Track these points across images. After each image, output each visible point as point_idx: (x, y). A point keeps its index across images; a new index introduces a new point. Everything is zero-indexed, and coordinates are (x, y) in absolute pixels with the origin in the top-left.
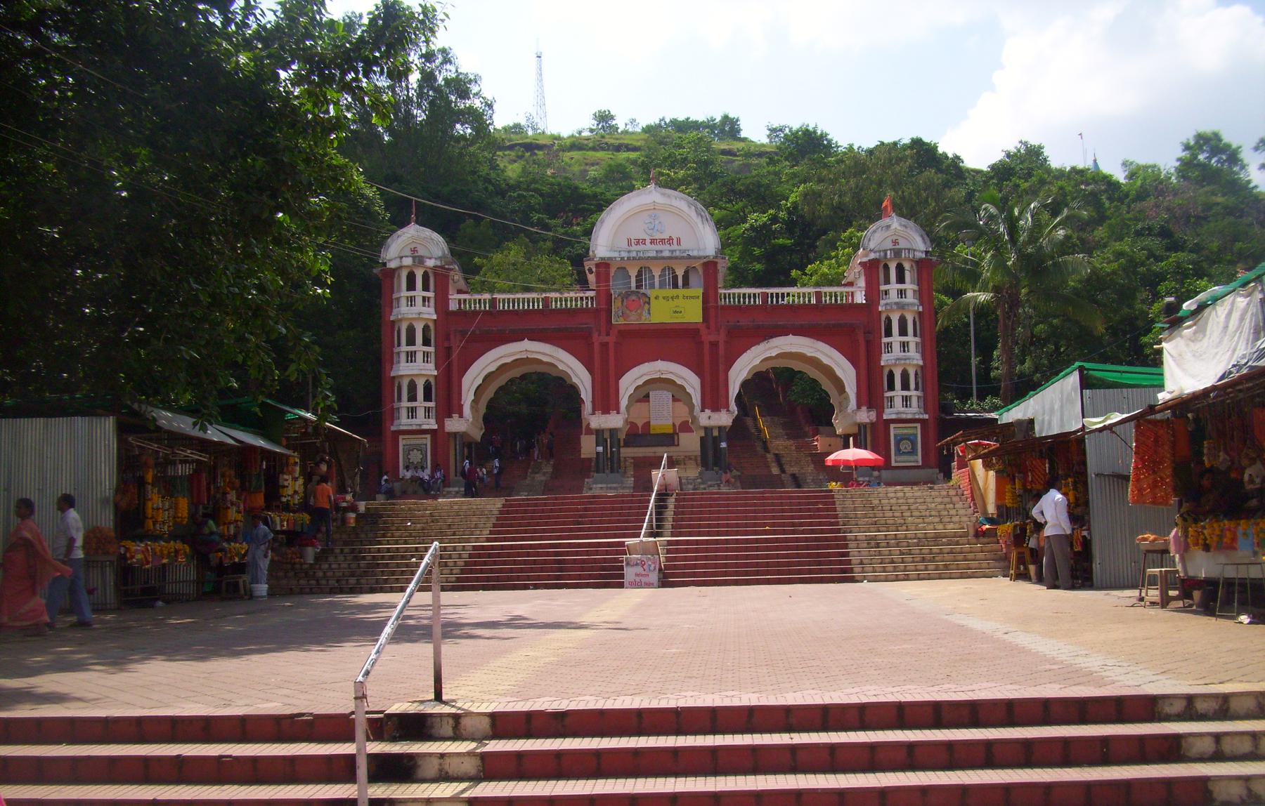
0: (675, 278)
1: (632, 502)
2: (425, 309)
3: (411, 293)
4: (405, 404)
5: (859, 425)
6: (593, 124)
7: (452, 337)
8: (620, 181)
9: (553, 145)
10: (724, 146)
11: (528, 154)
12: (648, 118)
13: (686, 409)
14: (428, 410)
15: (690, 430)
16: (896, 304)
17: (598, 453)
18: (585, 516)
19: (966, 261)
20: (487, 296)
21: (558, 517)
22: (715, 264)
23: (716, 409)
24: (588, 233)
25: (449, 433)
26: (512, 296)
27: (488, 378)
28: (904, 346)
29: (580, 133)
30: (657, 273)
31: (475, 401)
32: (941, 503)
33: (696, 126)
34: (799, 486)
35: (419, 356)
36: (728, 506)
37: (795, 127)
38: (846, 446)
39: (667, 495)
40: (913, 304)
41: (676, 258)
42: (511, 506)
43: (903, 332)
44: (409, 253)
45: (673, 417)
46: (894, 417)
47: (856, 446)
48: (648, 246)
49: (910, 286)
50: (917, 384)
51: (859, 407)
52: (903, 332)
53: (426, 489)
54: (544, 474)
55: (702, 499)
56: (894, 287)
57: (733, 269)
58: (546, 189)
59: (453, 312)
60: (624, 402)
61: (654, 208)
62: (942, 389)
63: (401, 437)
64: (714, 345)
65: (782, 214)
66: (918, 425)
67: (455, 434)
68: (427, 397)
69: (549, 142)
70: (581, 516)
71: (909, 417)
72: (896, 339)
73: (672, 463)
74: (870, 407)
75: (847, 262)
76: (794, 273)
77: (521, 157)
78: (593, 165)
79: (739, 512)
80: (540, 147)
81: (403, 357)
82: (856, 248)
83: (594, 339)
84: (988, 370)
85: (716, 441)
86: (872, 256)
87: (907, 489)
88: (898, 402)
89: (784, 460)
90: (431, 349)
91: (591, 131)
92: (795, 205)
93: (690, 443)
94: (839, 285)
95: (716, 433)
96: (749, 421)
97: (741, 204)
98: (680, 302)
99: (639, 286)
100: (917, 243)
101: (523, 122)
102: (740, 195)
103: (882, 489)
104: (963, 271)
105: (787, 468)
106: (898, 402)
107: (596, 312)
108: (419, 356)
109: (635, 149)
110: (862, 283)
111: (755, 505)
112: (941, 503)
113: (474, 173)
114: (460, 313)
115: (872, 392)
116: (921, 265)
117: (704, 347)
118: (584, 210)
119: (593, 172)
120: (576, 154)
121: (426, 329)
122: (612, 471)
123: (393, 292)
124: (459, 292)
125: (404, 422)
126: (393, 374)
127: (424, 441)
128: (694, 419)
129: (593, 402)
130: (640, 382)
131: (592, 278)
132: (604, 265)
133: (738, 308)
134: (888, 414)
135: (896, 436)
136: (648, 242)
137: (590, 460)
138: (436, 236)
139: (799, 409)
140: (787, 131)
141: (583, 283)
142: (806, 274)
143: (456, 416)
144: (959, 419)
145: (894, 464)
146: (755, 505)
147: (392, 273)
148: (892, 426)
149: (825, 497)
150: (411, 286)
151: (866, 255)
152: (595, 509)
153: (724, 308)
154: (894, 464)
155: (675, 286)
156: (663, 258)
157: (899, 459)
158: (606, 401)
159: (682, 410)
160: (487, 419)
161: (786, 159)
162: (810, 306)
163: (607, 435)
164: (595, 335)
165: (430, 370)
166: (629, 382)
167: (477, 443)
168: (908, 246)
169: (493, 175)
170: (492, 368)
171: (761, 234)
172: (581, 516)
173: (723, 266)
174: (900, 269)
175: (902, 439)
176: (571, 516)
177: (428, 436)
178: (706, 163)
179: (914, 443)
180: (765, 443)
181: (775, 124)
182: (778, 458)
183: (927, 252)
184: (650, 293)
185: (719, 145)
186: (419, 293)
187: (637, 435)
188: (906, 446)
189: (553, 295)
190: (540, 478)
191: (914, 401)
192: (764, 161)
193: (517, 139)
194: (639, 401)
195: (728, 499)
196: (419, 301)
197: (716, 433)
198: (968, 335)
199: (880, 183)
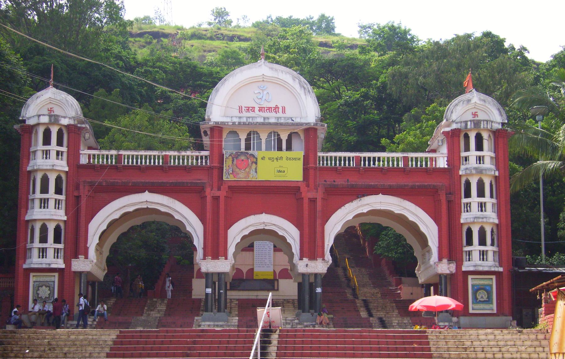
0: (280, 141)
1: (238, 337)
2: (59, 162)
4: (37, 244)
5: (440, 276)
6: (211, 19)
7: (81, 187)
8: (233, 62)
9: (176, 34)
10: (321, 39)
11: (155, 41)
12: (258, 14)
13: (286, 258)
14: (57, 251)
15: (289, 277)
16: (475, 169)
17: (207, 294)
18: (195, 349)
19: (536, 133)
20: (114, 152)
21: (168, 349)
22: (315, 130)
23: (313, 257)
24: (204, 105)
25: (75, 272)
26: (135, 153)
27: (113, 224)
28: (482, 206)
29: (200, 25)
30: (264, 137)
31: (100, 245)
32: (531, 346)
33: (297, 22)
34: (385, 327)
35: (52, 203)
36: (328, 343)
37: (383, 24)
38: (428, 294)
39: (271, 331)
40: (490, 170)
41: (281, 124)
42: (125, 337)
43: (481, 194)
44: (46, 112)
45: (274, 265)
46: (472, 269)
47: (436, 293)
49: (488, 153)
50: (493, 240)
51: (440, 259)
52: (481, 194)
53: (53, 320)
54: (159, 311)
55: (304, 336)
56: (473, 153)
57: (329, 138)
58: (169, 67)
59: (83, 166)
60: (231, 250)
61: (264, 79)
62: (515, 245)
63: (32, 274)
64: (313, 201)
65: (373, 92)
66: (494, 277)
67: (80, 273)
68: (57, 240)
69: (173, 32)
70: (190, 349)
71: (486, 269)
72: (474, 199)
73: (275, 304)
74: (450, 260)
75: (431, 133)
76: (383, 141)
77: (150, 43)
78: (210, 51)
79: (337, 349)
80: (166, 36)
81: (37, 203)
82: (439, 120)
83: (207, 194)
84: (555, 230)
85: (312, 287)
86: (454, 126)
87: (497, 332)
88: (476, 256)
89: (371, 306)
90: (62, 197)
91: (210, 24)
92: (384, 85)
93: (289, 288)
94: (423, 151)
95: (312, 280)
96: (340, 271)
97: (336, 84)
98: (284, 163)
99: (248, 147)
100: (493, 115)
101: (152, 16)
102: (336, 75)
103: (473, 332)
104: (534, 141)
105: (374, 312)
106: (476, 256)
107: (210, 169)
108: (52, 203)
109: (246, 40)
110: (444, 150)
111: (353, 343)
112: (531, 346)
113: (106, 50)
114: (89, 167)
115: (452, 248)
116: (497, 134)
117: (300, 203)
118: (201, 86)
119: (210, 57)
120: (195, 42)
121: (58, 180)
122: (219, 310)
123: (30, 146)
124: (90, 148)
125: (35, 261)
126: (27, 218)
127: (53, 279)
128: (293, 266)
129: (205, 248)
130: (246, 232)
131: (206, 140)
132: (217, 129)
133: (334, 170)
134: (467, 266)
135: (473, 286)
136: (257, 109)
137: (200, 300)
138: (71, 99)
139: (383, 262)
140: (375, 27)
141: (200, 147)
142: (394, 143)
143: (82, 257)
144: (530, 272)
145: (471, 311)
146: (353, 343)
147: (31, 130)
148: (470, 277)
149: (419, 337)
150: (47, 141)
151: (448, 126)
152: (203, 342)
153: (323, 169)
154: (471, 311)
155: (280, 149)
156: (270, 124)
157: (476, 306)
158: (216, 249)
159: (282, 258)
160: (110, 261)
161: (375, 50)
162: (398, 170)
163: (215, 278)
165: (61, 215)
166: (237, 232)
167: (100, 283)
168: (486, 118)
169: (124, 53)
170: (117, 216)
171: (354, 107)
172: (190, 349)
173: (321, 135)
174: (479, 138)
176: (181, 349)
177: (56, 275)
178: (305, 50)
179: (489, 293)
180: (354, 290)
181: (365, 23)
182: (366, 303)
183: (503, 124)
184: (259, 154)
185: (317, 38)
186: (54, 147)
187: (241, 280)
188: (482, 295)
189: (172, 153)
190: (155, 314)
191: (490, 255)
192: (357, 51)
193: (146, 28)
194: (244, 250)
195: (329, 337)
196: (53, 154)
197: (312, 280)
198: (537, 199)
199: (459, 66)
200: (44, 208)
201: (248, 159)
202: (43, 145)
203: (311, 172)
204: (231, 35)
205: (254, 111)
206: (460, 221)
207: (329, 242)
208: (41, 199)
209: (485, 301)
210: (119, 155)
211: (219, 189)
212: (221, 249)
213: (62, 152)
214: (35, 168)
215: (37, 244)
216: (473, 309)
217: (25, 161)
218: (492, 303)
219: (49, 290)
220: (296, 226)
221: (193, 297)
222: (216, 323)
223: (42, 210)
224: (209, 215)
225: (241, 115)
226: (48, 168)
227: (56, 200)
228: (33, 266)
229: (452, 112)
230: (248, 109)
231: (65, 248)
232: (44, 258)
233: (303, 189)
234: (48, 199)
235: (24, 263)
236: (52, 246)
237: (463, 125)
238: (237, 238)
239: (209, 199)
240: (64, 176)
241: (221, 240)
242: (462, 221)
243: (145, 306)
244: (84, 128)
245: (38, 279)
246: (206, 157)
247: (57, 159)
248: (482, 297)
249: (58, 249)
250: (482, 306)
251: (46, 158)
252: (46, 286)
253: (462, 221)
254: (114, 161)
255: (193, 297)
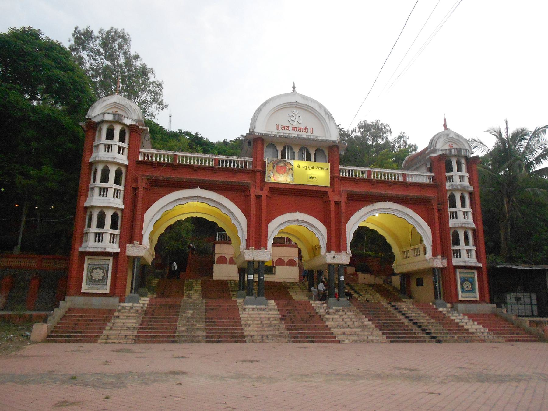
3: (109, 142)
4: (94, 229)
7: (139, 180)
14: (113, 236)
20: (170, 153)
25: (128, 257)
35: (111, 192)
48: (291, 131)
51: (435, 255)
60: (270, 242)
63: (87, 258)
64: (337, 203)
67: (134, 258)
68: (114, 226)
71: (473, 265)
81: (97, 191)
83: (251, 192)
90: (121, 188)
114: (148, 164)
123: (94, 140)
125: (91, 244)
126: (86, 204)
127: (107, 262)
129: (248, 240)
134: (456, 262)
136: (291, 128)
147: (94, 127)
148: (458, 271)
150: (110, 136)
153: (345, 179)
158: (257, 239)
160: (158, 248)
164: (252, 189)
165: (119, 203)
166: (275, 227)
175: (465, 280)
177: (111, 258)
179: (472, 284)
200: (103, 196)
201: (286, 165)
202: (97, 227)
203: (336, 180)
204: (68, 298)
205: (288, 130)
206: (114, 259)
207: (350, 238)
208: (96, 233)
209: (470, 291)
210: (175, 155)
211: (262, 189)
212: (263, 240)
213: (124, 148)
214: (97, 159)
215: (94, 229)
216: (462, 297)
217: (88, 153)
218: (475, 292)
219: (103, 272)
220: (324, 225)
221: (215, 278)
222: (258, 307)
223: (102, 198)
224: (253, 212)
225: (279, 131)
226: (110, 160)
227: (115, 190)
228: (88, 249)
229: (436, 143)
230: (284, 128)
231: (120, 235)
232: (100, 243)
233: (330, 193)
234: (107, 188)
235: (81, 246)
236: (108, 232)
237: (448, 152)
238: (275, 231)
239: (253, 198)
240: (123, 170)
241: (263, 232)
242: (450, 226)
243: (183, 286)
244: (144, 130)
245: (93, 262)
246: (249, 162)
247: (119, 152)
248: (467, 287)
249: (114, 235)
250: (468, 294)
251: (108, 151)
252: (101, 269)
253: (450, 226)
254: (170, 160)
255: (215, 278)
